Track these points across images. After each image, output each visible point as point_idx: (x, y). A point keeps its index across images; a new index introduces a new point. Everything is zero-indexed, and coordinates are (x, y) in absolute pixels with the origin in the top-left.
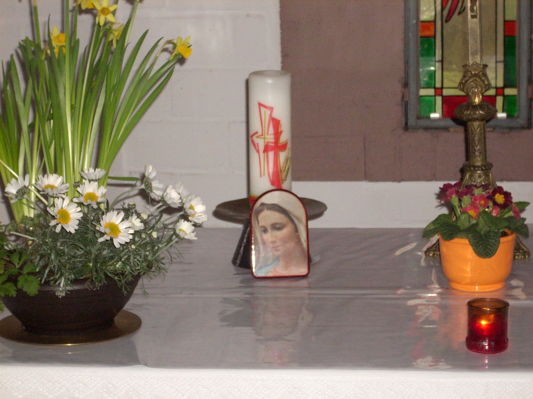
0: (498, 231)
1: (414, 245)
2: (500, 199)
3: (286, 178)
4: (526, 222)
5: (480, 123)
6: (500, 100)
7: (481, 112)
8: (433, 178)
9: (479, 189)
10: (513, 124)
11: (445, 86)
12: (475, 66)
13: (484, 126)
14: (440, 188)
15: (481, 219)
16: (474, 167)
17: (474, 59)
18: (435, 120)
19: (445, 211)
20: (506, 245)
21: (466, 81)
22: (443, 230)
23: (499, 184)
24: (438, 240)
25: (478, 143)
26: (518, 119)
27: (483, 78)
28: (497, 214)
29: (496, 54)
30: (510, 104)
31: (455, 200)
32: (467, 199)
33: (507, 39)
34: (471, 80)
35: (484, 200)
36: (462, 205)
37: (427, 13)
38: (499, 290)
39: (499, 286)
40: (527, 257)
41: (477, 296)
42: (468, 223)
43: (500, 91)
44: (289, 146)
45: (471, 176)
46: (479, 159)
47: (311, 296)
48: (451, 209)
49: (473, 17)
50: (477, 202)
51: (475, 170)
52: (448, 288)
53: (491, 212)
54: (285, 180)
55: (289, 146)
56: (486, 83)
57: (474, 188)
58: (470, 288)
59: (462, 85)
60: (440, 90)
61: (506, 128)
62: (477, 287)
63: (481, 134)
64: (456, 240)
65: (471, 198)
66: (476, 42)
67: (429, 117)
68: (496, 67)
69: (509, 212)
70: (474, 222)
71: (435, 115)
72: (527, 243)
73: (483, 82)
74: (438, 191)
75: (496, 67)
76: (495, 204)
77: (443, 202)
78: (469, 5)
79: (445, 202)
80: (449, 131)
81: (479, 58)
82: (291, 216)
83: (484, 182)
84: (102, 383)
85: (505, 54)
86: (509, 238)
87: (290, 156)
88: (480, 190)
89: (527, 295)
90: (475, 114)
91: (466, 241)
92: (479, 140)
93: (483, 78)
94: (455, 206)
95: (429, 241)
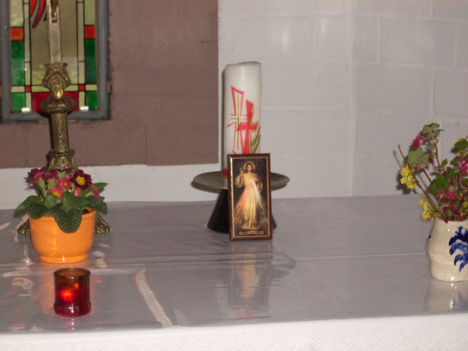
0: (80, 209)
1: (7, 225)
2: (81, 180)
4: (105, 201)
5: (62, 114)
6: (82, 95)
8: (28, 166)
9: (62, 173)
10: (94, 115)
11: (33, 83)
12: (56, 65)
13: (66, 116)
14: (28, 173)
15: (65, 199)
16: (59, 153)
17: (56, 59)
18: (26, 114)
19: (33, 193)
20: (87, 221)
21: (49, 79)
23: (80, 168)
24: (28, 220)
25: (61, 133)
26: (98, 112)
27: (64, 75)
28: (79, 194)
29: (78, 55)
30: (91, 99)
31: (41, 183)
32: (52, 182)
33: (87, 41)
34: (52, 78)
36: (48, 187)
38: (84, 260)
40: (107, 231)
41: (63, 267)
42: (53, 203)
43: (82, 87)
46: (62, 146)
48: (40, 192)
49: (54, 21)
50: (61, 184)
52: (38, 261)
53: (73, 193)
56: (67, 79)
57: (58, 172)
58: (57, 261)
59: (45, 82)
61: (88, 119)
63: (63, 124)
64: (44, 218)
65: (56, 181)
67: (20, 112)
68: (78, 67)
69: (89, 191)
70: (59, 201)
71: (26, 110)
72: (106, 219)
73: (64, 78)
74: (26, 175)
75: (78, 67)
76: (77, 185)
77: (31, 185)
78: (50, 11)
79: (34, 185)
80: (38, 123)
81: (60, 58)
83: (68, 166)
84: (435, 340)
85: (85, 55)
90: (57, 107)
91: (52, 219)
92: (62, 129)
93: (64, 75)
94: (42, 189)
95: (22, 220)
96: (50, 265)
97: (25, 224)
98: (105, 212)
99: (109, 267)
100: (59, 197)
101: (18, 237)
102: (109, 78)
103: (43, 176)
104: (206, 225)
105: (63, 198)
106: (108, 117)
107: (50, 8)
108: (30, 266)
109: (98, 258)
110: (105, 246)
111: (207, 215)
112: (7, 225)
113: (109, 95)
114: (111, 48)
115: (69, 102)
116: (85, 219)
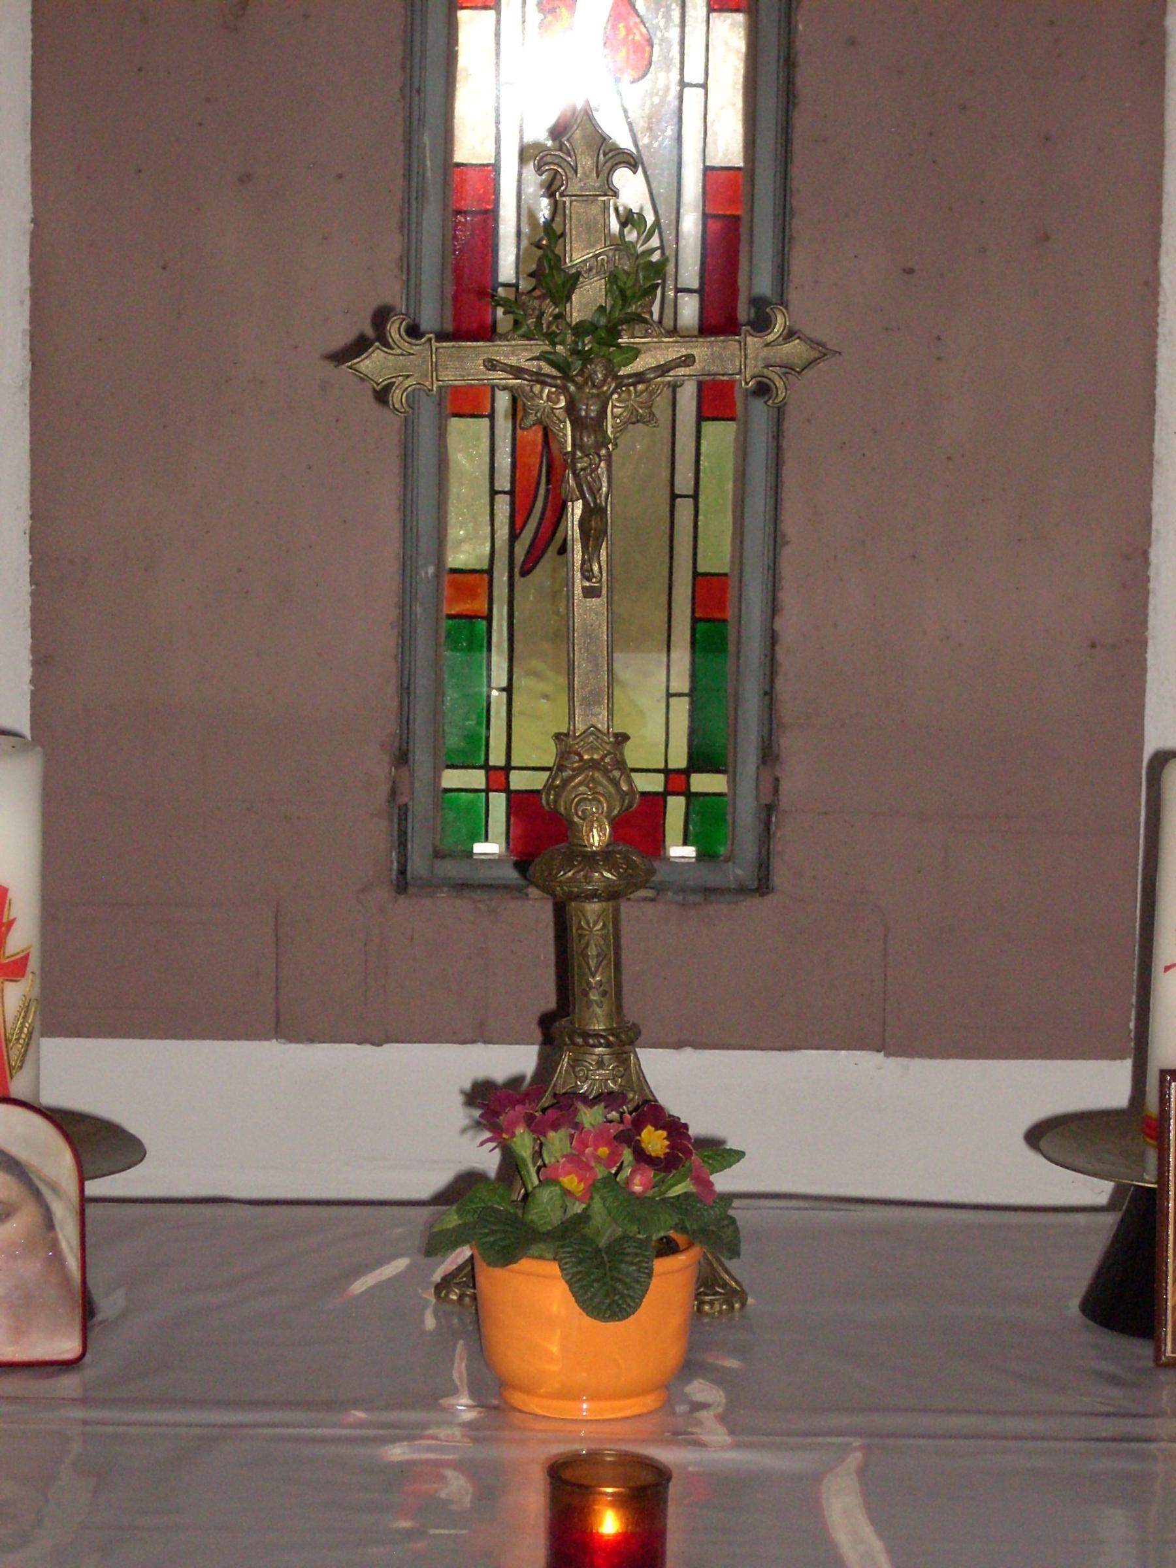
0: (649, 1238)
1: (402, 1264)
2: (654, 1140)
3: (23, 1061)
5: (604, 904)
6: (676, 806)
7: (606, 874)
10: (709, 876)
15: (597, 1204)
16: (586, 1035)
18: (489, 862)
20: (670, 1280)
21: (566, 782)
22: (487, 1235)
24: (472, 1257)
25: (597, 968)
26: (730, 864)
28: (648, 1186)
30: (706, 819)
32: (558, 1142)
33: (701, 626)
35: (608, 1144)
37: (465, 547)
39: (649, 1402)
40: (737, 1306)
42: (559, 1213)
44: (34, 964)
45: (575, 1063)
46: (598, 1010)
47: (88, 1428)
51: (587, 1044)
53: (628, 1181)
54: (21, 1068)
55: (34, 964)
57: (580, 1106)
60: (502, 773)
61: (694, 891)
62: (585, 1406)
64: (524, 1264)
66: (597, 666)
67: (470, 853)
70: (578, 1208)
71: (488, 849)
72: (738, 1269)
73: (616, 784)
76: (641, 1156)
82: (32, 1176)
83: (615, 1082)
86: (681, 1259)
87: (36, 993)
88: (599, 1109)
89: (731, 1433)
90: (588, 879)
91: (554, 1268)
93: (617, 774)
94: (524, 1161)
96: (540, 1425)
97: (460, 1268)
98: (735, 1253)
99: (736, 1446)
100: (579, 1195)
101: (435, 1313)
102: (769, 755)
103: (530, 1121)
104: (1075, 1304)
105: (591, 1198)
106: (762, 885)
107: (578, 547)
108: (469, 1425)
109: (705, 1406)
110: (732, 1363)
111: (1079, 1265)
112: (402, 1264)
113: (768, 811)
114: (780, 655)
115: (630, 864)
116: (663, 1274)
